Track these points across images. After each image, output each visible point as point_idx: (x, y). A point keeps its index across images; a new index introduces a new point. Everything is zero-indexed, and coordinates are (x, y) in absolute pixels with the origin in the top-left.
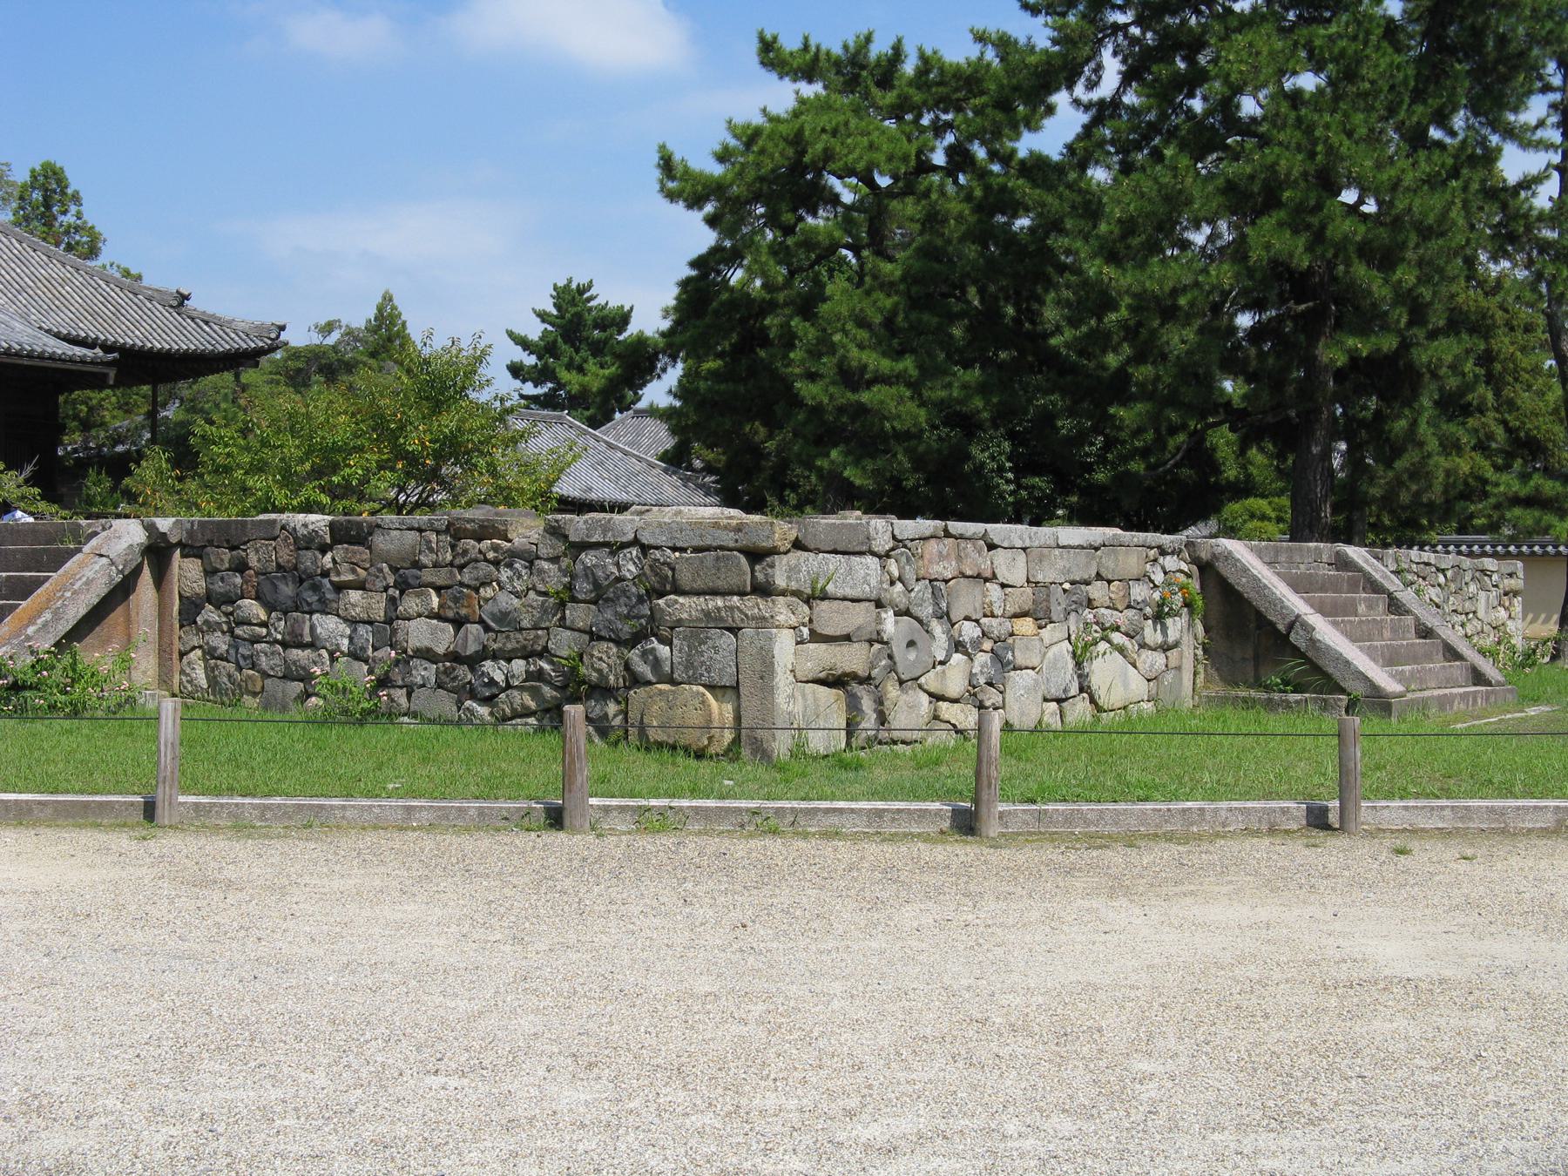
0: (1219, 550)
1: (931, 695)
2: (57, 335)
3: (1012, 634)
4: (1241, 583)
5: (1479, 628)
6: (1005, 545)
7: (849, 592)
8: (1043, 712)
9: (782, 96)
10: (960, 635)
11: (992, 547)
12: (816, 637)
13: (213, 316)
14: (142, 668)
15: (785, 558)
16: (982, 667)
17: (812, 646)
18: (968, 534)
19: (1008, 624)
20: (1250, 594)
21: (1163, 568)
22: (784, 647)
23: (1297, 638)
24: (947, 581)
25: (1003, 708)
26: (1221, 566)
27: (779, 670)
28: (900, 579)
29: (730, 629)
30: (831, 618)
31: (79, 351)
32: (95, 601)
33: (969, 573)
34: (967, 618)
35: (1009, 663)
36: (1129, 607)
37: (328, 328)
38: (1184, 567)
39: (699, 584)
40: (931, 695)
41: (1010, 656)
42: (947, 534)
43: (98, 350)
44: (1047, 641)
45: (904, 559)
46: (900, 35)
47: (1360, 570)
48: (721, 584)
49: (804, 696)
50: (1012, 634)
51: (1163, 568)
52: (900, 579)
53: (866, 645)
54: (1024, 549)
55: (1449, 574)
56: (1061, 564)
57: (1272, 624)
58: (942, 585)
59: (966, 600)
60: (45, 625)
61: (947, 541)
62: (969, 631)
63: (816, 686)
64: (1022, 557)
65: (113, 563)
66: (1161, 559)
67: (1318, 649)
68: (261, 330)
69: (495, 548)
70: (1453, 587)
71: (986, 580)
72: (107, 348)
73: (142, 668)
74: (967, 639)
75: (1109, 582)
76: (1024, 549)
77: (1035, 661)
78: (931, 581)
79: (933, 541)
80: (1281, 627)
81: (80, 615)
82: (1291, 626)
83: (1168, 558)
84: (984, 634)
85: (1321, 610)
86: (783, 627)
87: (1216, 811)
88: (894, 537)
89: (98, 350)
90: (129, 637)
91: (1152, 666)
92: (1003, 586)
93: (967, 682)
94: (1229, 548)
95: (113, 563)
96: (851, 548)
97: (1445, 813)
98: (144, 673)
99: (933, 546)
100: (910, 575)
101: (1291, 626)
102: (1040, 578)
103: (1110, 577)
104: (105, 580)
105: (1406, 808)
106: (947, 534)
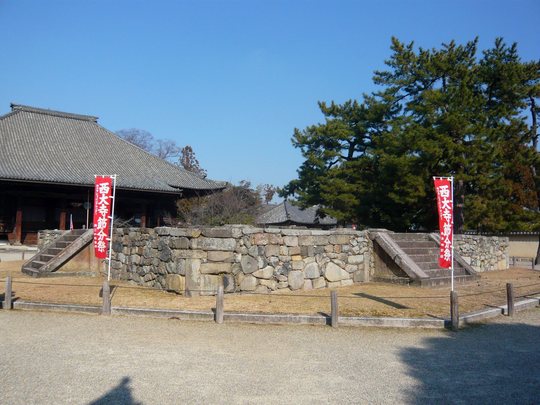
0: (377, 236)
1: (257, 278)
2: (173, 187)
3: (292, 260)
4: (382, 245)
5: (491, 257)
6: (289, 235)
7: (222, 249)
8: (305, 282)
9: (537, 134)
10: (270, 261)
11: (283, 236)
12: (209, 261)
13: (211, 180)
14: (93, 265)
15: (196, 239)
16: (279, 270)
17: (207, 264)
18: (274, 232)
19: (290, 257)
20: (385, 248)
21: (357, 241)
22: (196, 265)
23: (397, 261)
24: (264, 246)
25: (288, 281)
26: (377, 240)
27: (194, 271)
28: (244, 245)
29: (184, 259)
30: (215, 256)
31: (174, 189)
32: (78, 249)
33: (273, 243)
34: (273, 256)
35: (290, 268)
36: (342, 252)
37: (242, 182)
38: (366, 240)
39: (179, 247)
40: (257, 278)
41: (290, 266)
42: (265, 232)
43: (178, 189)
44: (306, 263)
45: (246, 239)
46: (333, 100)
47: (434, 241)
48: (183, 247)
49: (205, 278)
50: (292, 260)
51: (357, 241)
52: (244, 245)
53: (230, 264)
54: (297, 236)
55: (478, 241)
56: (312, 240)
57: (390, 257)
58: (262, 247)
59: (272, 251)
60: (64, 255)
61: (265, 234)
62: (273, 260)
63: (210, 275)
64: (297, 238)
65: (83, 240)
66: (356, 239)
67: (402, 264)
68: (222, 183)
69: (147, 236)
70: (480, 245)
71: (281, 245)
72: (181, 188)
73: (93, 265)
74: (272, 262)
75: (334, 245)
76: (297, 236)
77: (302, 268)
78: (258, 245)
79: (259, 234)
80: (392, 258)
81: (74, 253)
82: (395, 258)
83: (359, 238)
84: (279, 260)
85: (407, 252)
86: (195, 259)
87: (295, 318)
88: (242, 233)
89: (178, 189)
90: (90, 258)
91: (351, 269)
92: (288, 246)
93: (272, 274)
94: (380, 235)
95: (83, 240)
96: (223, 236)
97: (372, 321)
98: (94, 267)
99: (259, 236)
100: (248, 244)
101: (395, 258)
102: (304, 244)
103: (334, 244)
104: (81, 244)
105: (358, 319)
106: (265, 232)
